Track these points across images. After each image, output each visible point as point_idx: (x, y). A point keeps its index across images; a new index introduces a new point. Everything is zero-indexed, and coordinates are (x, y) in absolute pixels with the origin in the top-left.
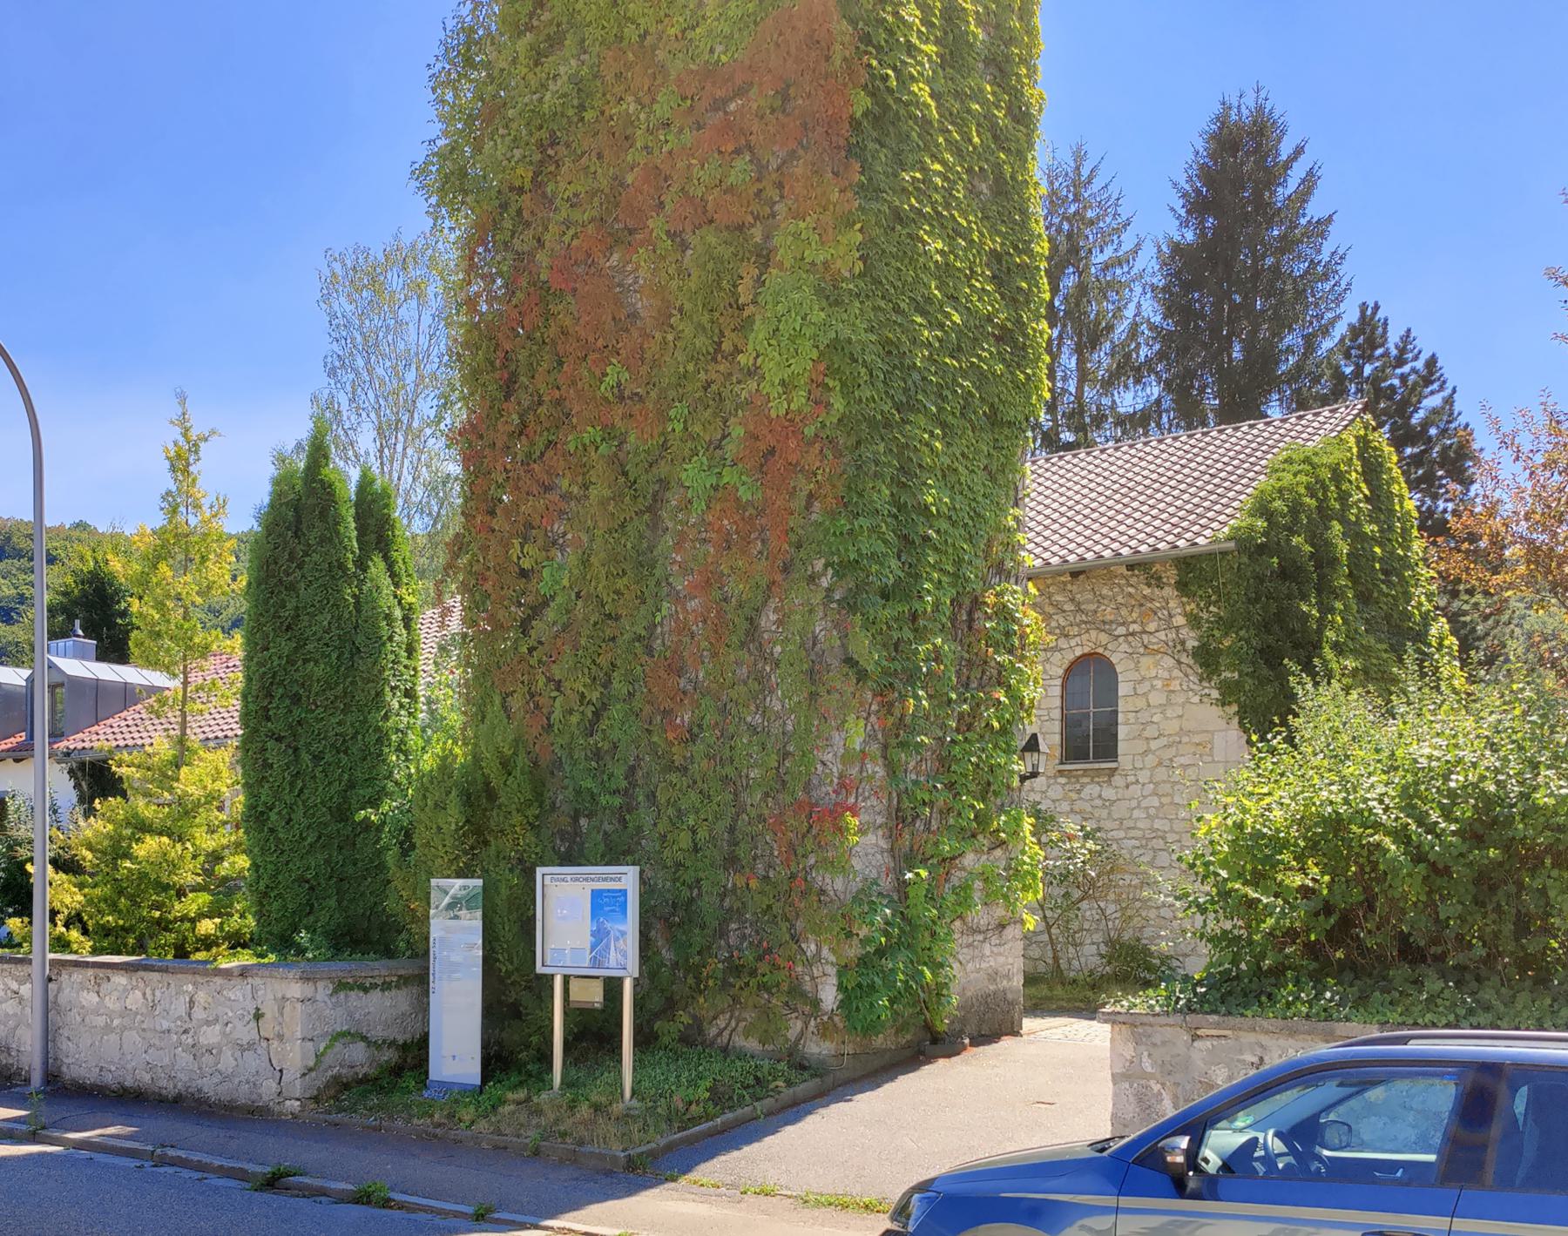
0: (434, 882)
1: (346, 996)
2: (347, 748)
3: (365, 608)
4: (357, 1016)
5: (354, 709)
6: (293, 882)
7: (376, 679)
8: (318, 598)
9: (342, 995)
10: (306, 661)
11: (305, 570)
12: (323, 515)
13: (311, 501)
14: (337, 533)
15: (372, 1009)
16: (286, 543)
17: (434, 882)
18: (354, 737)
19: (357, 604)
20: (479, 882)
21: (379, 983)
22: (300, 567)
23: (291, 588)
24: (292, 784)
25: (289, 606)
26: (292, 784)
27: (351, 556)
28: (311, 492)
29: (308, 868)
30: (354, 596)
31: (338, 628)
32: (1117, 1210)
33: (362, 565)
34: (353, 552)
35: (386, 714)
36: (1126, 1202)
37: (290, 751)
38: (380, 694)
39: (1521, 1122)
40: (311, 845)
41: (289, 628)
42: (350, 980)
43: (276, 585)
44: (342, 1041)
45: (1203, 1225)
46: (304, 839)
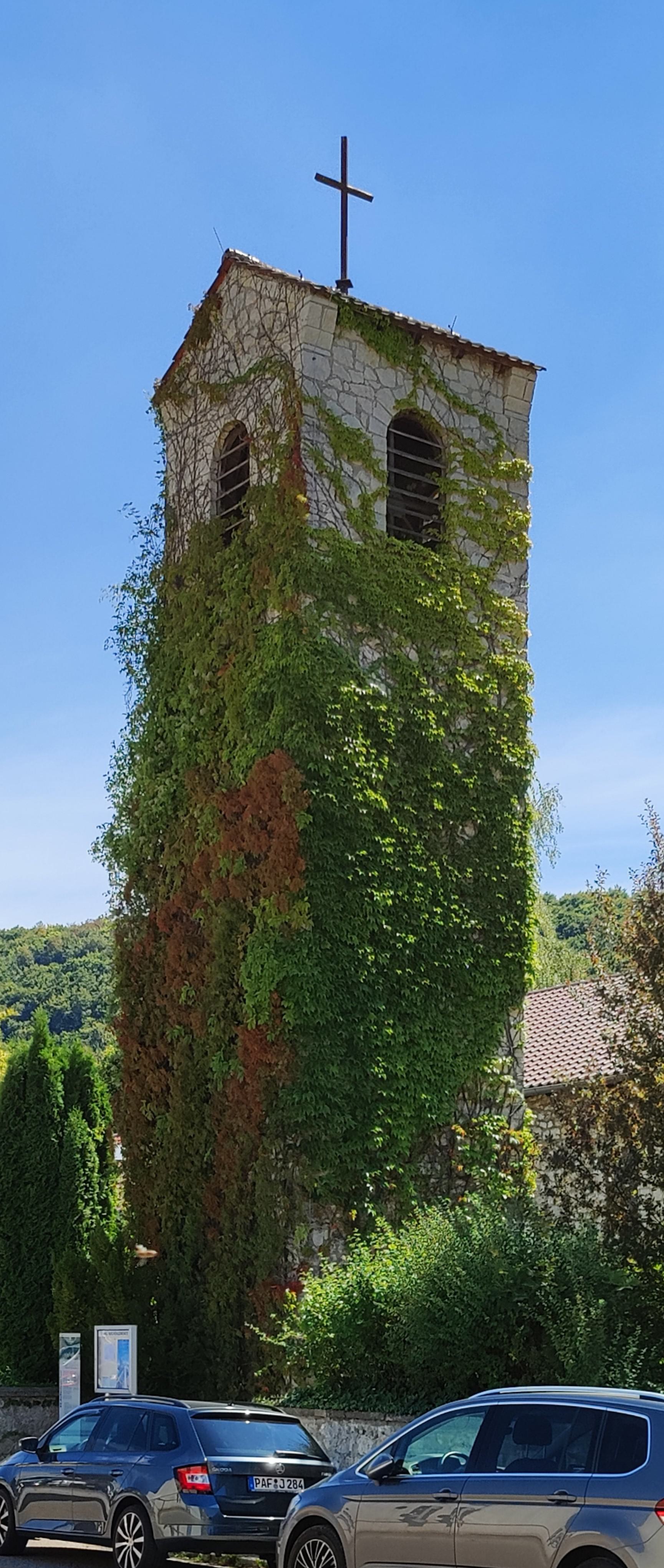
0: (61, 1335)
1: (15, 1410)
2: (54, 1243)
3: (65, 1145)
4: (23, 1422)
5: (58, 1216)
6: (14, 1335)
7: (72, 1195)
8: (34, 1140)
9: (12, 1408)
10: (26, 1184)
11: (27, 1121)
12: (39, 1084)
13: (33, 1073)
14: (48, 1094)
15: (35, 1418)
16: (14, 1104)
17: (61, 1335)
18: (58, 1235)
19: (61, 1145)
20: (78, 1335)
21: (42, 1401)
22: (24, 1119)
23: (17, 1134)
24: (15, 1269)
25: (15, 1147)
26: (15, 1269)
27: (56, 1110)
28: (33, 1068)
29: (25, 1326)
30: (58, 1137)
31: (47, 1160)
32: (360, 1501)
33: (64, 1115)
34: (58, 1107)
35: (80, 1217)
36: (364, 1498)
37: (14, 1247)
38: (75, 1205)
39: (145, 1428)
40: (27, 1309)
41: (15, 1161)
42: (18, 1399)
43: (6, 1133)
44: (11, 1437)
45: (474, 1511)
46: (23, 1306)
